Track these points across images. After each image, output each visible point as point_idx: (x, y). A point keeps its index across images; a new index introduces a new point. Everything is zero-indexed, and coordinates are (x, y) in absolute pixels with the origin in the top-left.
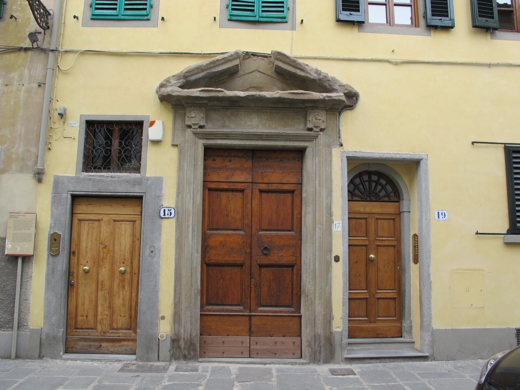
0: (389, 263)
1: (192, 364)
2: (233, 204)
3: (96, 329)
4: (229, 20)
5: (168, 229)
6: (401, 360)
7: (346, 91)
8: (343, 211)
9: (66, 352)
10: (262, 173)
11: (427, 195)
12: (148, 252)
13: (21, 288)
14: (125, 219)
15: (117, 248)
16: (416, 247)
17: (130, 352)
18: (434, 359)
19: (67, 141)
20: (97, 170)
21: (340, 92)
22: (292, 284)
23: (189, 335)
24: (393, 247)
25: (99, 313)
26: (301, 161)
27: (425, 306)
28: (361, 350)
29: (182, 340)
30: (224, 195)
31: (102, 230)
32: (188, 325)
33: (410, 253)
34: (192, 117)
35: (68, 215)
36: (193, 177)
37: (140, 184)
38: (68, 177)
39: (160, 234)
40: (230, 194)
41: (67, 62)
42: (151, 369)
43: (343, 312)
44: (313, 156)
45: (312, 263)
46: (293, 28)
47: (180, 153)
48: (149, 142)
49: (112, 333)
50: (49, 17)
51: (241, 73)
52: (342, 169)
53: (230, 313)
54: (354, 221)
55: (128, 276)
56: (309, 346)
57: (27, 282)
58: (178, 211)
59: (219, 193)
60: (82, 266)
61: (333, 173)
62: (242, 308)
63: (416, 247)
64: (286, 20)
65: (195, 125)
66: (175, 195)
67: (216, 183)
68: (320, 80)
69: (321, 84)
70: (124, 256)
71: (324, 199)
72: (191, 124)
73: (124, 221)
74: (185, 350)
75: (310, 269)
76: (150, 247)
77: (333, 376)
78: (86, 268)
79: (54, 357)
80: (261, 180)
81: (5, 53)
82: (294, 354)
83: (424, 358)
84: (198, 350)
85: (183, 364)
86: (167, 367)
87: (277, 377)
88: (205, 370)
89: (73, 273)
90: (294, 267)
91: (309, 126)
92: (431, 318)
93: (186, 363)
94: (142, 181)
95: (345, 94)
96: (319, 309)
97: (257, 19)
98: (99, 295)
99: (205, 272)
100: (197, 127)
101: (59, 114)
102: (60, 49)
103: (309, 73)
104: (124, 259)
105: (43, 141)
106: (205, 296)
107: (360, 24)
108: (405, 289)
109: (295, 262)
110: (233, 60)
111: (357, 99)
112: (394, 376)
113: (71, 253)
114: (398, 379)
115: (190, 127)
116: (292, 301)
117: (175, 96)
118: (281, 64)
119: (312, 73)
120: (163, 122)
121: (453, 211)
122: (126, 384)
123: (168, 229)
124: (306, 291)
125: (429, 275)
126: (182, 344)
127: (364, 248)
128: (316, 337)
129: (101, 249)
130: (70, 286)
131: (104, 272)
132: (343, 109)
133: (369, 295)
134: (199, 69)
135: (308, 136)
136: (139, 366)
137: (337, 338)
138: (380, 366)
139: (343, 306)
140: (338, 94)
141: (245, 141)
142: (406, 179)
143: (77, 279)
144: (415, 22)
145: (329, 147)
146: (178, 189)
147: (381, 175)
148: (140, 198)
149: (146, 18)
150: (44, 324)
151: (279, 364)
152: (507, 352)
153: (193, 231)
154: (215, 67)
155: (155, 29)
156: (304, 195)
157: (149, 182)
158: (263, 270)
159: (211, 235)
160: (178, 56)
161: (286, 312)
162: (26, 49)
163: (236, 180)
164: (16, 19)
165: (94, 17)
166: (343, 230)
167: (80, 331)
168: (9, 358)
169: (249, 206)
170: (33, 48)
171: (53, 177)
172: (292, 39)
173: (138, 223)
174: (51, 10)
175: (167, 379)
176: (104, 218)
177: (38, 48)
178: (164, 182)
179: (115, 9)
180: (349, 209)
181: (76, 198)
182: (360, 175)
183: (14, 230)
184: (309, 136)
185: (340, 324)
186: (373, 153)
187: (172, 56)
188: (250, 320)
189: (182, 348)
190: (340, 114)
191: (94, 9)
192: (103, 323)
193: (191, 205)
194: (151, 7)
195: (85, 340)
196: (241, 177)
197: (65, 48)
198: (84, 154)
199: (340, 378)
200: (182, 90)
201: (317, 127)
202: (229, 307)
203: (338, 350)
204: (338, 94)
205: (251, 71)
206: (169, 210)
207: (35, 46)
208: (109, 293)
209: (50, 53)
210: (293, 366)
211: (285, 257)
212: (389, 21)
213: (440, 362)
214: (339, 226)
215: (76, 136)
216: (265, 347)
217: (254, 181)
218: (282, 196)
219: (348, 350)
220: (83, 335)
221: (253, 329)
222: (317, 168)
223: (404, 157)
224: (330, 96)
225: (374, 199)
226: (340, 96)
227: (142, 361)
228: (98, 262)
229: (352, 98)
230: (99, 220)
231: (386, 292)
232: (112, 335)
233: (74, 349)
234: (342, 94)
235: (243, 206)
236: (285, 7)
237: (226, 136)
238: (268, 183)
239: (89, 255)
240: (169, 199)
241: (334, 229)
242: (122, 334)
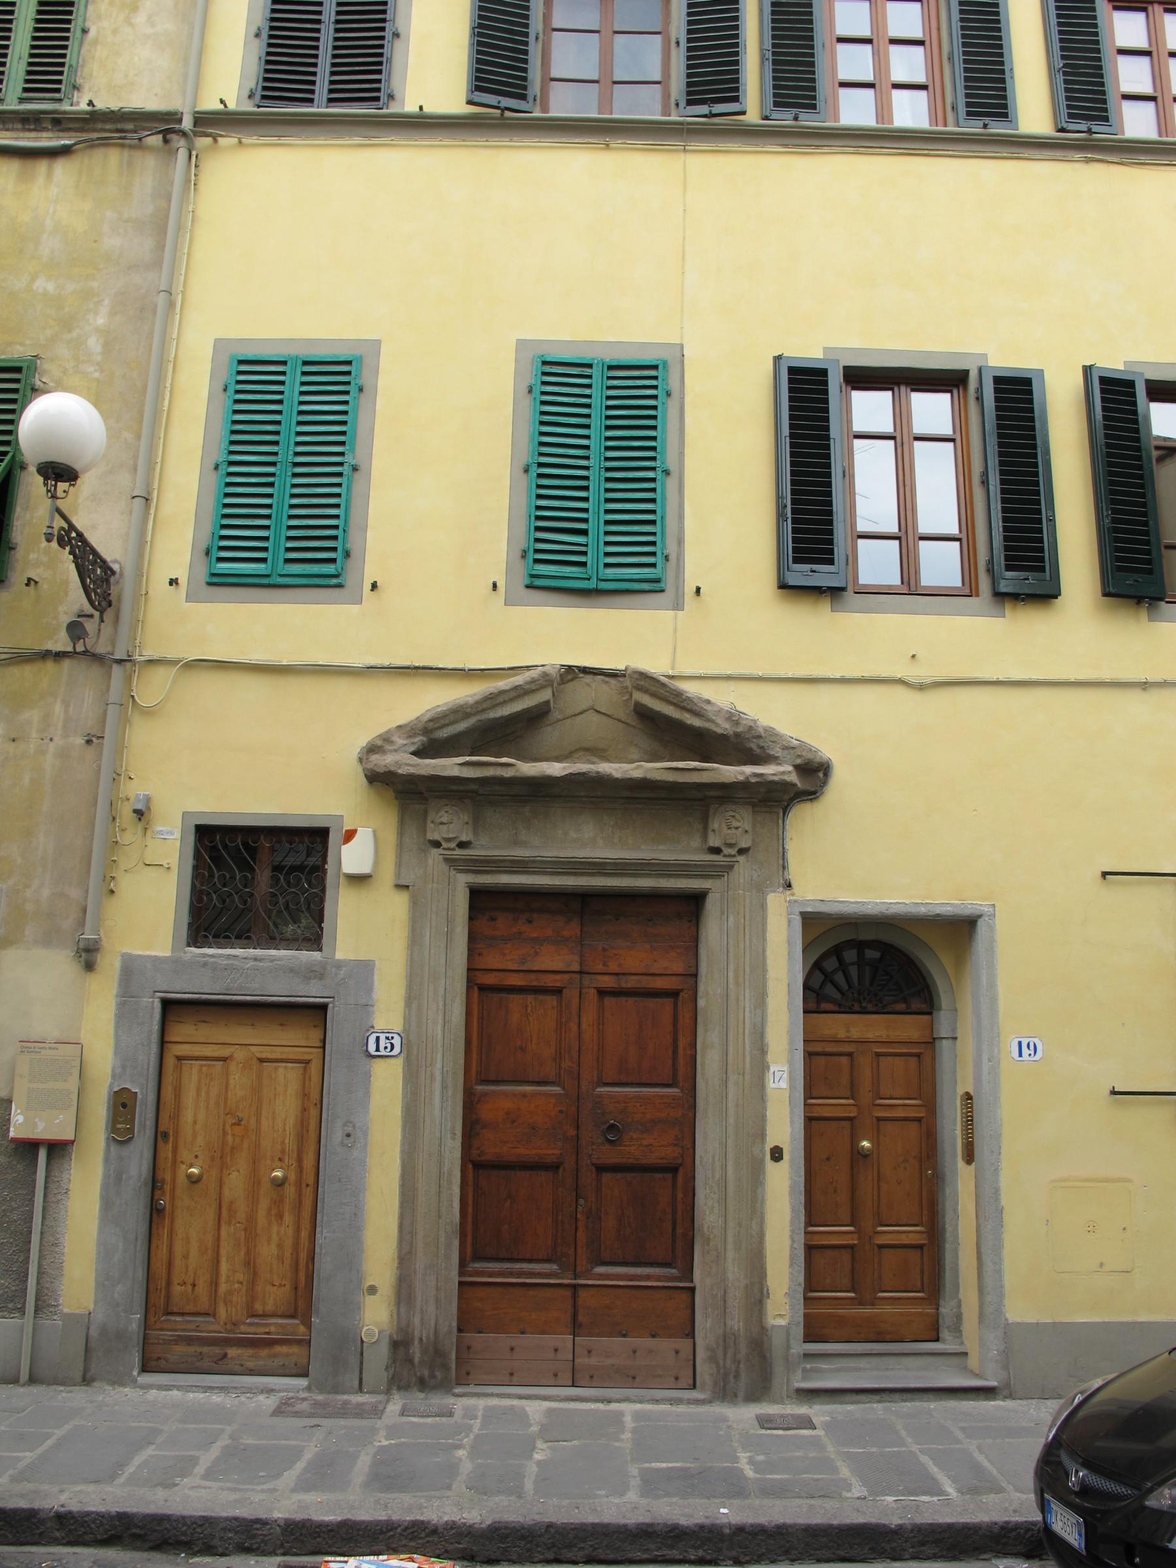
0: (906, 1161)
1: (438, 1400)
2: (535, 1021)
3: (214, 1316)
4: (527, 587)
5: (387, 1083)
6: (931, 1396)
7: (799, 761)
8: (791, 1042)
9: (146, 1367)
10: (604, 950)
11: (994, 1000)
12: (338, 1136)
13: (44, 1218)
14: (284, 1056)
15: (265, 1124)
16: (969, 1120)
17: (294, 1372)
18: (1011, 1396)
19: (152, 873)
20: (222, 941)
21: (785, 762)
22: (674, 1212)
23: (432, 1331)
24: (916, 1124)
25: (223, 1279)
27: (989, 1267)
28: (838, 1370)
29: (416, 1342)
30: (515, 1000)
31: (232, 1082)
32: (431, 1309)
33: (955, 1139)
34: (442, 823)
35: (154, 1048)
36: (443, 961)
37: (321, 976)
38: (155, 959)
39: (367, 1094)
40: (530, 998)
41: (152, 688)
42: (344, 1412)
43: (791, 1280)
44: (723, 913)
45: (718, 1164)
46: (678, 605)
47: (415, 904)
48: (342, 879)
49: (250, 1324)
50: (112, 580)
51: (555, 715)
52: (790, 943)
53: (528, 1281)
54: (822, 1061)
55: (290, 1191)
56: (712, 1359)
57: (58, 1202)
58: (409, 1041)
59: (504, 995)
60: (184, 1167)
61: (768, 953)
62: (555, 1267)
63: (969, 1120)
64: (662, 585)
65: (449, 840)
66: (401, 1004)
67: (497, 974)
68: (737, 735)
69: (743, 744)
70: (283, 1143)
71: (747, 1013)
74: (423, 1366)
75: (713, 1177)
76: (345, 1125)
77: (763, 1431)
78: (194, 1170)
79: (119, 1380)
81: (9, 665)
82: (677, 1378)
83: (987, 1392)
84: (453, 1366)
85: (418, 1398)
86: (380, 1407)
87: (634, 1431)
88: (470, 1414)
89: (163, 1181)
90: (678, 1172)
91: (714, 841)
92: (1001, 1296)
93: (425, 1399)
94: (325, 969)
95: (797, 767)
96: (734, 1272)
97: (592, 584)
98: (223, 1233)
99: (471, 1183)
100: (453, 845)
101: (135, 811)
102: (137, 657)
103: (713, 721)
104: (283, 1151)
105: (95, 874)
106: (469, 1239)
107: (834, 593)
108: (944, 1224)
109: (680, 1161)
110: (538, 690)
112: (903, 1433)
113: (160, 1136)
114: (910, 1440)
115: (437, 844)
116: (673, 1251)
119: (719, 721)
120: (374, 832)
121: (1032, 1053)
122: (294, 1443)
123: (387, 1083)
124: (705, 1229)
125: (997, 1191)
126: (416, 1351)
127: (846, 1124)
128: (727, 1339)
129: (228, 1127)
130: (156, 1213)
131: (236, 1182)
132: (792, 800)
133: (859, 1239)
134: (458, 712)
135: (710, 866)
136: (316, 1404)
137: (777, 1341)
138: (877, 1409)
139: (791, 1265)
140: (781, 769)
141: (565, 878)
142: (946, 960)
143: (173, 1198)
144: (970, 589)
145: (761, 890)
146: (410, 988)
147: (887, 949)
148: (321, 1009)
149: (334, 581)
150: (96, 1302)
151: (641, 1402)
152: (1111, 1377)
153: (444, 1087)
155: (355, 608)
156: (701, 1003)
157: (342, 972)
158: (607, 1177)
160: (408, 675)
161: (659, 1279)
162: (59, 656)
164: (36, 582)
165: (216, 580)
166: (792, 1087)
167: (178, 1319)
168: (15, 1381)
169: (574, 1028)
170: (76, 653)
171: (119, 958)
172: (675, 631)
173: (314, 1068)
174: (116, 561)
175: (383, 1433)
176: (235, 1055)
177: (85, 653)
178: (376, 972)
179: (264, 560)
181: (173, 1008)
182: (837, 951)
183: (30, 1081)
184: (712, 866)
185: (785, 1309)
186: (864, 903)
187: (400, 673)
188: (575, 1297)
189: (416, 1360)
190: (786, 810)
191: (214, 559)
192: (231, 1302)
193: (440, 1028)
194: (347, 554)
195: (189, 1341)
196: (554, 960)
197: (149, 653)
198: (192, 904)
199: (777, 1436)
200: (419, 761)
201: (731, 845)
202: (525, 1266)
203: (778, 1369)
204: (781, 769)
206: (387, 1038)
207: (80, 648)
208: (245, 1230)
209: (115, 667)
210: (674, 1408)
211: (660, 1149)
212: (905, 580)
213: (1024, 1402)
214: (783, 1078)
215: (174, 861)
216: (609, 1361)
217: (586, 969)
218: (652, 1003)
219: (805, 1370)
220: (184, 1330)
221: (580, 1318)
222: (731, 942)
223: (938, 910)
224: (762, 775)
225: (870, 1007)
226: (783, 773)
227: (321, 1393)
228: (221, 1158)
229: (814, 774)
230: (224, 1059)
231: (898, 1232)
232: (252, 1329)
233: (162, 1363)
234: (790, 768)
236: (659, 554)
238: (617, 974)
239: (200, 1140)
240: (388, 1014)
241: (771, 1085)
242: (275, 1326)
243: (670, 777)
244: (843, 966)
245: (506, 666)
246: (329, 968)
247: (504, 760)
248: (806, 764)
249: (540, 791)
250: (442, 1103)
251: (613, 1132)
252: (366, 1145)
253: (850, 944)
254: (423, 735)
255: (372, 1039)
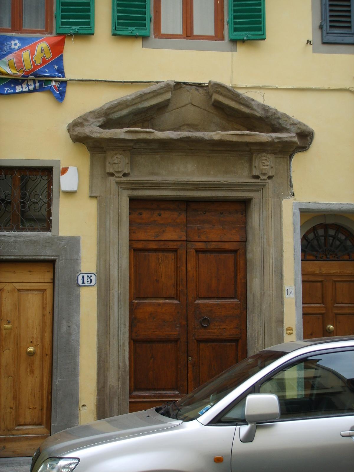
2: (164, 267)
5: (88, 299)
7: (299, 131)
8: (296, 275)
10: (198, 229)
26: (244, 214)
30: (152, 256)
34: (115, 164)
40: (160, 254)
55: (37, 359)
59: (147, 254)
65: (119, 172)
67: (143, 242)
68: (267, 117)
69: (269, 121)
72: (113, 172)
73: (31, 290)
80: (197, 238)
91: (255, 172)
100: (121, 175)
110: (164, 93)
111: (312, 139)
115: (112, 175)
117: (94, 138)
118: (221, 99)
119: (258, 110)
120: (77, 168)
123: (88, 299)
127: (320, 317)
148: (52, 262)
153: (119, 301)
154: (141, 102)
158: (202, 345)
159: (138, 305)
163: (167, 238)
166: (296, 298)
169: (184, 269)
176: (5, 288)
180: (303, 270)
182: (314, 229)
186: (331, 204)
190: (291, 157)
202: (162, 393)
205: (183, 105)
206: (88, 276)
211: (229, 330)
218: (223, 256)
224: (280, 138)
226: (291, 137)
229: (305, 138)
234: (295, 135)
235: (177, 269)
237: (156, 186)
238: (205, 242)
240: (88, 262)
243: (235, 139)
244: (317, 237)
245: (145, 81)
246: (56, 240)
247: (148, 130)
248: (302, 132)
249: (166, 147)
250: (119, 309)
251: (205, 323)
252: (79, 332)
253: (321, 226)
254: (104, 117)
255: (80, 277)
